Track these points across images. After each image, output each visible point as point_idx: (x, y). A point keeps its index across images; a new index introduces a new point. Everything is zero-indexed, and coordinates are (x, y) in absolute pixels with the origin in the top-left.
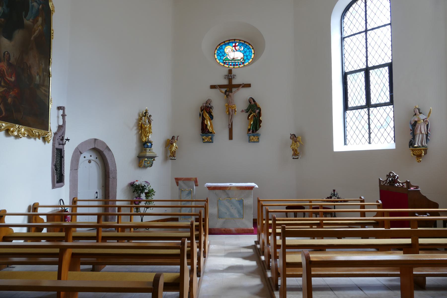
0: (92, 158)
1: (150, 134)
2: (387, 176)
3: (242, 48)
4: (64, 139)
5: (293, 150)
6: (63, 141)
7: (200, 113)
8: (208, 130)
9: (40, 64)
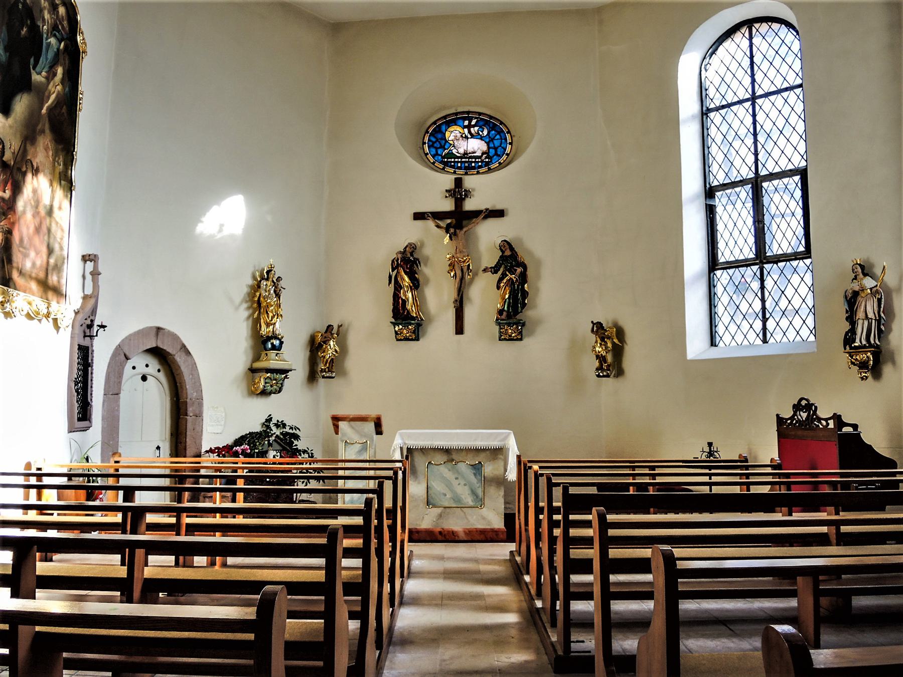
0: (150, 370)
1: (278, 320)
2: (794, 406)
3: (485, 132)
4: (93, 325)
5: (598, 357)
6: (92, 329)
7: (390, 273)
8: (408, 312)
9: (56, 163)
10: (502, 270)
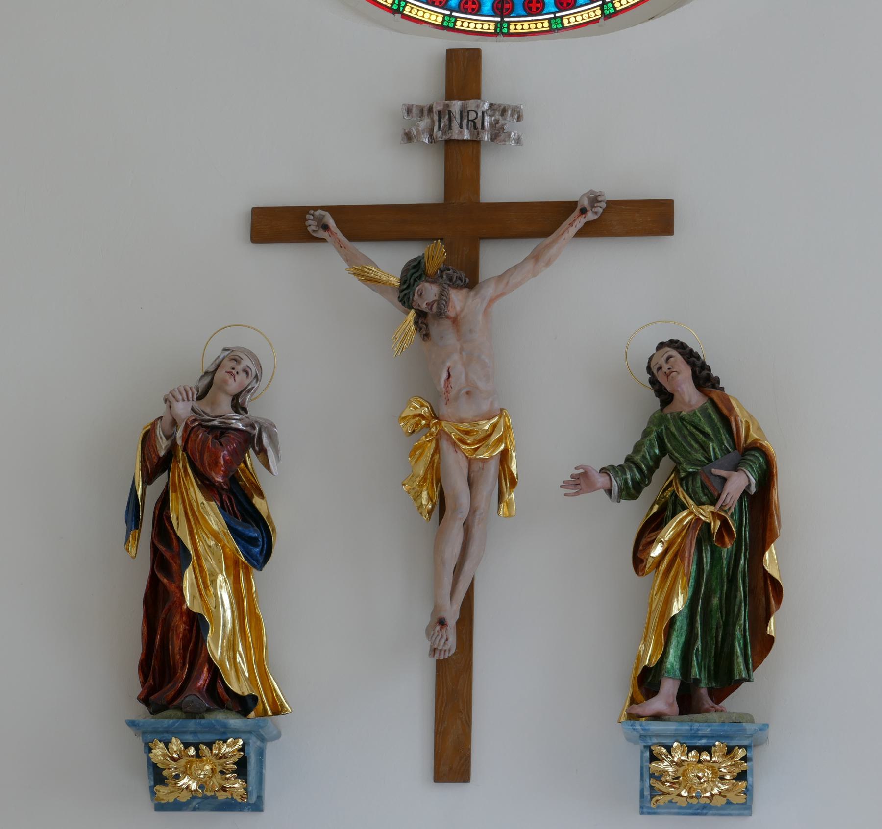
10: (659, 478)
